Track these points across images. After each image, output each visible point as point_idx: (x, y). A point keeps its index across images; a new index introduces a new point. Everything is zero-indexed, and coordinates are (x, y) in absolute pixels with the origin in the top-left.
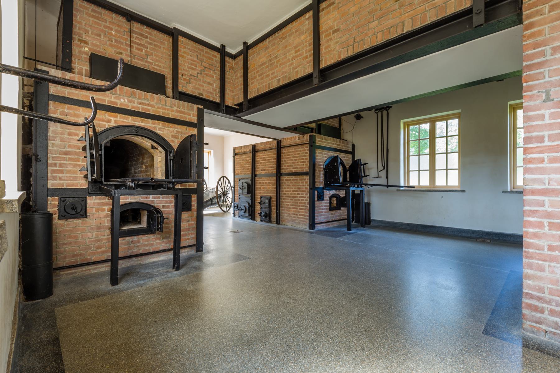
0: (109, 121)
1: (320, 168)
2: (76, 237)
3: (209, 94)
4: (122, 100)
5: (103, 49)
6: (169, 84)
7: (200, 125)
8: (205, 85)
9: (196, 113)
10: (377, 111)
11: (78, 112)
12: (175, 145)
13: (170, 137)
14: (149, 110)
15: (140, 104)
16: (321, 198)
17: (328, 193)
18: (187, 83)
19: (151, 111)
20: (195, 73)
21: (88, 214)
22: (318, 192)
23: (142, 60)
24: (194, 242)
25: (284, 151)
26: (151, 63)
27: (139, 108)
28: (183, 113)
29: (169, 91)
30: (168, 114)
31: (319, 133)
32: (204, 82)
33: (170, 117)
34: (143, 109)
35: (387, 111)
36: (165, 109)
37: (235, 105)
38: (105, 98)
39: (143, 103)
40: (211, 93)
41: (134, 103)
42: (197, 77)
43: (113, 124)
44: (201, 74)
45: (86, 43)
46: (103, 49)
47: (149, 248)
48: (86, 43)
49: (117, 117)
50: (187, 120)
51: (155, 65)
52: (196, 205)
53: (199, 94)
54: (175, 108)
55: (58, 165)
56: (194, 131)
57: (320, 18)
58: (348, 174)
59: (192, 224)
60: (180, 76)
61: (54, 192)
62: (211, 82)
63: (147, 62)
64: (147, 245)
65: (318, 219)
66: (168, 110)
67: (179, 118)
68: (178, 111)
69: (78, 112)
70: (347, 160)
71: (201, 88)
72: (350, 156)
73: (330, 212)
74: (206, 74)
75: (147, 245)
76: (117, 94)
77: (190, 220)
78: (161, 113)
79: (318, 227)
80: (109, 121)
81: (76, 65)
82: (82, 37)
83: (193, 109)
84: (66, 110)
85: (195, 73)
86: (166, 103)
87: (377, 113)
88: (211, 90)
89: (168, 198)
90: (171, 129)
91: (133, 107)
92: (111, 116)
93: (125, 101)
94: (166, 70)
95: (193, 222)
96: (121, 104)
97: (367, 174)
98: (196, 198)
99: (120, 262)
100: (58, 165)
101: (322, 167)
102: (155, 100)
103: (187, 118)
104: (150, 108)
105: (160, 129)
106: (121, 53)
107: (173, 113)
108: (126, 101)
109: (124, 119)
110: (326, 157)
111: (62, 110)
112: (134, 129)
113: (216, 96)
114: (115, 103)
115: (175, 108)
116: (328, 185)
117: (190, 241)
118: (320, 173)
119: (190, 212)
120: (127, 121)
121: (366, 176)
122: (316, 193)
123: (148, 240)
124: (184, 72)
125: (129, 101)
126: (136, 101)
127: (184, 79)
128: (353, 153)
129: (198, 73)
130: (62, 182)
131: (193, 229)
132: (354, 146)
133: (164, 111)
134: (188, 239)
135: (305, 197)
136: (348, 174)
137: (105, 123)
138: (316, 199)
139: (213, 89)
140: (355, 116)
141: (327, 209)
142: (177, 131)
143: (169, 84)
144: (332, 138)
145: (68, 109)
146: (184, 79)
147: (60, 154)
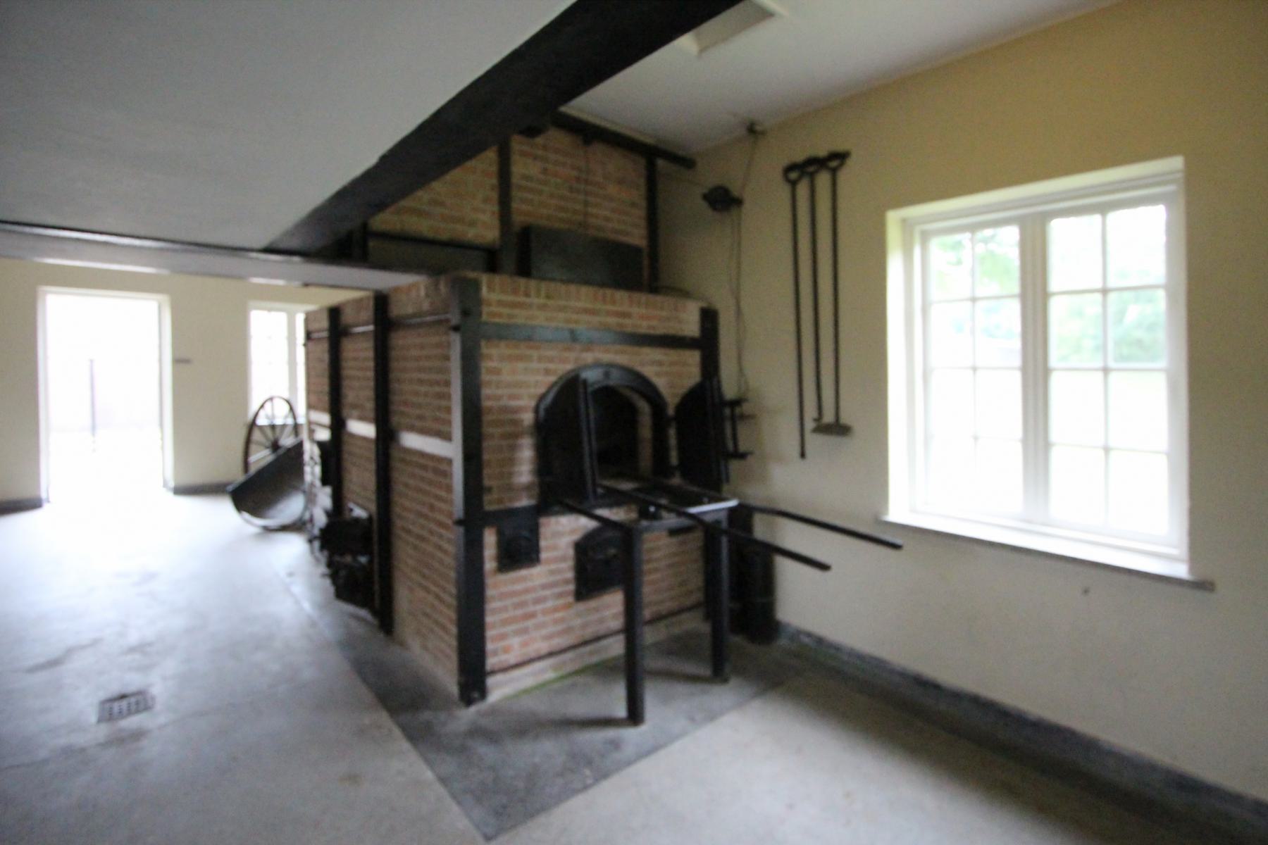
1: (516, 423)
10: (793, 175)
16: (520, 552)
17: (563, 532)
22: (500, 534)
25: (401, 341)
31: (524, 270)
35: (834, 171)
58: (672, 432)
65: (503, 644)
70: (673, 375)
72: (693, 359)
73: (582, 606)
79: (500, 689)
87: (793, 184)
97: (742, 448)
101: (528, 418)
110: (547, 372)
116: (558, 492)
118: (513, 448)
121: (743, 456)
122: (490, 539)
128: (707, 343)
132: (709, 317)
135: (445, 552)
136: (672, 432)
138: (490, 564)
141: (560, 595)
144: (585, 290)
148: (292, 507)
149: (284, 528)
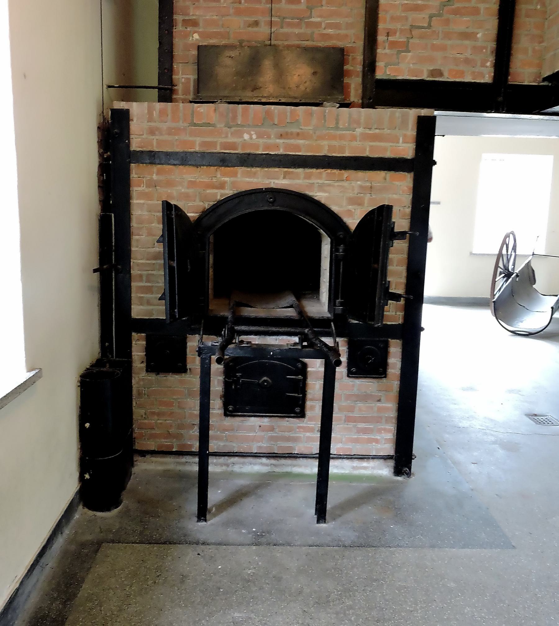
0: (222, 186)
2: (170, 404)
3: (461, 68)
4: (246, 137)
5: (223, 26)
6: (355, 65)
7: (421, 166)
8: (449, 42)
9: (411, 131)
11: (173, 177)
12: (352, 222)
13: (344, 203)
14: (298, 147)
15: (281, 136)
18: (399, 52)
19: (304, 148)
20: (421, 18)
21: (188, 367)
23: (298, 25)
24: (389, 449)
26: (318, 25)
27: (277, 147)
29: (354, 85)
32: (448, 35)
33: (347, 154)
34: (287, 147)
36: (334, 138)
37: (544, 79)
38: (215, 140)
39: (287, 133)
40: (467, 61)
41: (269, 137)
42: (430, 26)
43: (229, 192)
44: (439, 15)
45: (195, 23)
46: (223, 26)
47: (289, 444)
48: (195, 23)
49: (235, 175)
51: (329, 26)
52: (399, 365)
53: (433, 73)
54: (359, 131)
55: (144, 278)
56: (396, 191)
57: (47, 539)
59: (386, 409)
60: (381, 38)
61: (143, 325)
62: (470, 30)
63: (308, 25)
64: (288, 439)
66: (341, 137)
68: (366, 137)
69: (173, 177)
71: (439, 55)
74: (457, 12)
75: (288, 439)
76: (238, 125)
77: (383, 399)
78: (324, 149)
80: (222, 186)
81: (180, 76)
82: (188, 15)
83: (404, 122)
84: (155, 177)
85: (421, 18)
86: (337, 123)
88: (468, 54)
90: (346, 184)
91: (267, 147)
92: (224, 175)
93: (251, 135)
94: (351, 32)
96: (245, 144)
99: (332, 463)
100: (144, 278)
102: (314, 121)
103: (388, 151)
104: (301, 142)
105: (321, 188)
106: (256, 23)
107: (354, 144)
108: (254, 137)
109: (249, 177)
111: (148, 177)
113: (483, 65)
114: (233, 146)
115: (359, 131)
117: (379, 446)
119: (384, 380)
120: (255, 180)
123: (290, 430)
124: (391, 26)
125: (259, 136)
126: (273, 132)
127: (393, 45)
129: (431, 17)
130: (152, 307)
131: (387, 420)
134: (377, 441)
137: (215, 191)
139: (474, 48)
142: (361, 187)
143: (355, 65)
145: (157, 174)
146: (393, 45)
147: (147, 260)
148: (537, 317)
149: (529, 335)
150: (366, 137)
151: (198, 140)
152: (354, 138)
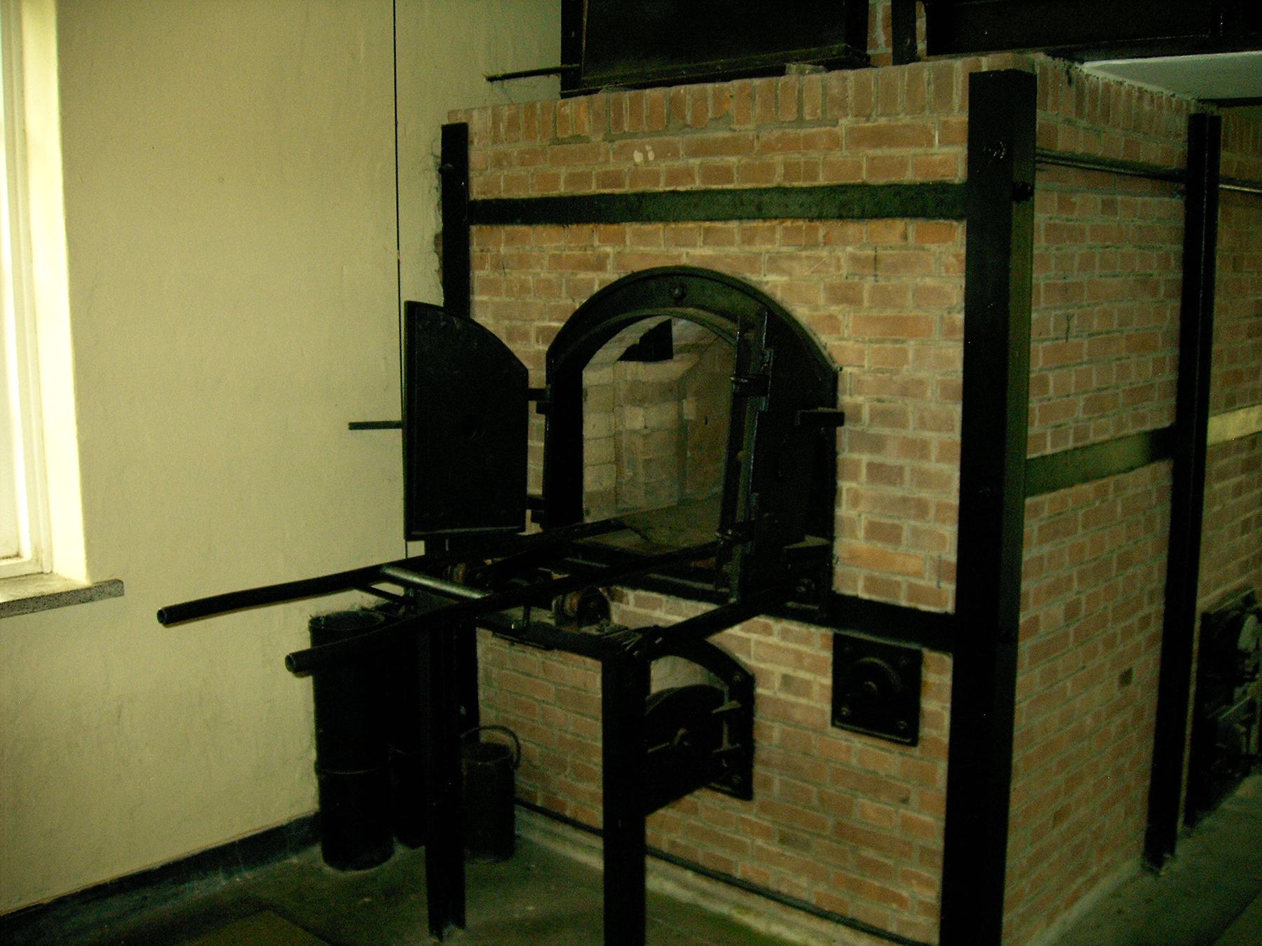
0: (600, 265)
13: (822, 299)
28: (879, 137)
30: (811, 172)
50: (909, 176)
58: (535, 467)
64: (722, 841)
66: (809, 143)
67: (864, 177)
68: (859, 138)
89: (807, 640)
90: (824, 253)
95: (927, 818)
98: (947, 679)
105: (775, 263)
107: (837, 156)
112: (749, 306)
114: (615, 178)
115: (846, 122)
133: (794, 157)
134: (901, 901)
136: (535, 467)
140: (1255, 602)
142: (855, 259)
150: (859, 138)
151: (563, 171)
152: (835, 142)
